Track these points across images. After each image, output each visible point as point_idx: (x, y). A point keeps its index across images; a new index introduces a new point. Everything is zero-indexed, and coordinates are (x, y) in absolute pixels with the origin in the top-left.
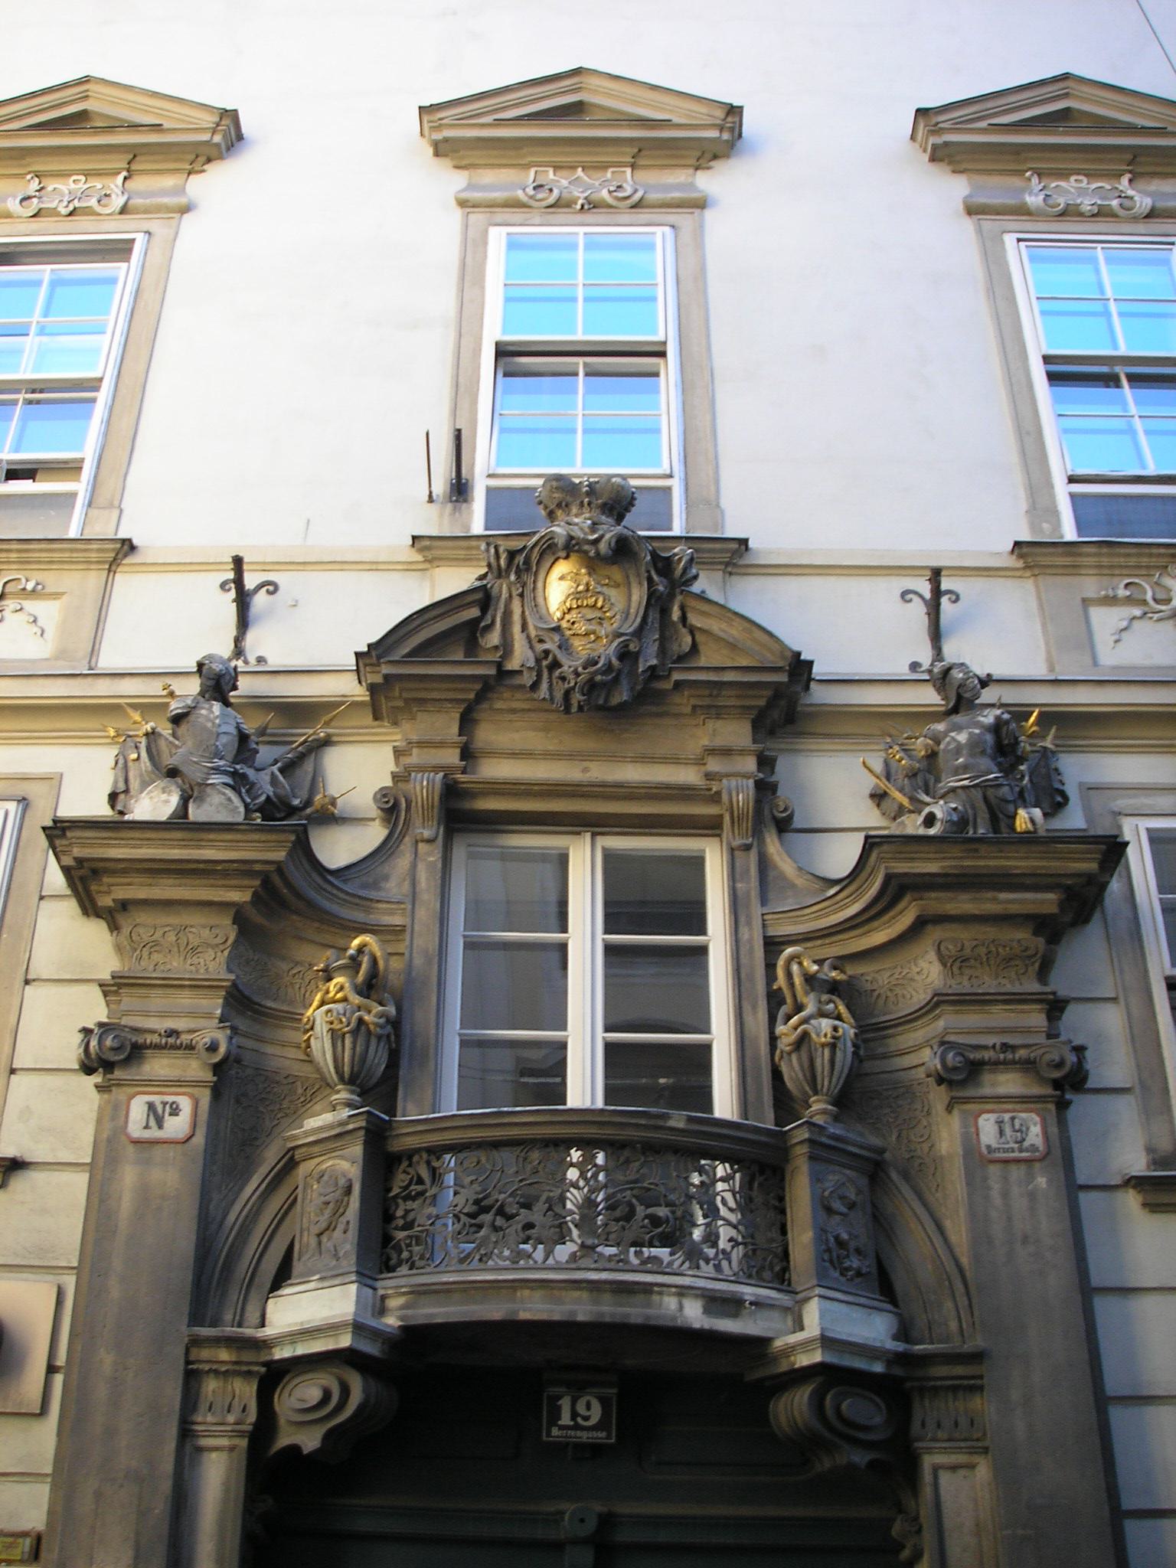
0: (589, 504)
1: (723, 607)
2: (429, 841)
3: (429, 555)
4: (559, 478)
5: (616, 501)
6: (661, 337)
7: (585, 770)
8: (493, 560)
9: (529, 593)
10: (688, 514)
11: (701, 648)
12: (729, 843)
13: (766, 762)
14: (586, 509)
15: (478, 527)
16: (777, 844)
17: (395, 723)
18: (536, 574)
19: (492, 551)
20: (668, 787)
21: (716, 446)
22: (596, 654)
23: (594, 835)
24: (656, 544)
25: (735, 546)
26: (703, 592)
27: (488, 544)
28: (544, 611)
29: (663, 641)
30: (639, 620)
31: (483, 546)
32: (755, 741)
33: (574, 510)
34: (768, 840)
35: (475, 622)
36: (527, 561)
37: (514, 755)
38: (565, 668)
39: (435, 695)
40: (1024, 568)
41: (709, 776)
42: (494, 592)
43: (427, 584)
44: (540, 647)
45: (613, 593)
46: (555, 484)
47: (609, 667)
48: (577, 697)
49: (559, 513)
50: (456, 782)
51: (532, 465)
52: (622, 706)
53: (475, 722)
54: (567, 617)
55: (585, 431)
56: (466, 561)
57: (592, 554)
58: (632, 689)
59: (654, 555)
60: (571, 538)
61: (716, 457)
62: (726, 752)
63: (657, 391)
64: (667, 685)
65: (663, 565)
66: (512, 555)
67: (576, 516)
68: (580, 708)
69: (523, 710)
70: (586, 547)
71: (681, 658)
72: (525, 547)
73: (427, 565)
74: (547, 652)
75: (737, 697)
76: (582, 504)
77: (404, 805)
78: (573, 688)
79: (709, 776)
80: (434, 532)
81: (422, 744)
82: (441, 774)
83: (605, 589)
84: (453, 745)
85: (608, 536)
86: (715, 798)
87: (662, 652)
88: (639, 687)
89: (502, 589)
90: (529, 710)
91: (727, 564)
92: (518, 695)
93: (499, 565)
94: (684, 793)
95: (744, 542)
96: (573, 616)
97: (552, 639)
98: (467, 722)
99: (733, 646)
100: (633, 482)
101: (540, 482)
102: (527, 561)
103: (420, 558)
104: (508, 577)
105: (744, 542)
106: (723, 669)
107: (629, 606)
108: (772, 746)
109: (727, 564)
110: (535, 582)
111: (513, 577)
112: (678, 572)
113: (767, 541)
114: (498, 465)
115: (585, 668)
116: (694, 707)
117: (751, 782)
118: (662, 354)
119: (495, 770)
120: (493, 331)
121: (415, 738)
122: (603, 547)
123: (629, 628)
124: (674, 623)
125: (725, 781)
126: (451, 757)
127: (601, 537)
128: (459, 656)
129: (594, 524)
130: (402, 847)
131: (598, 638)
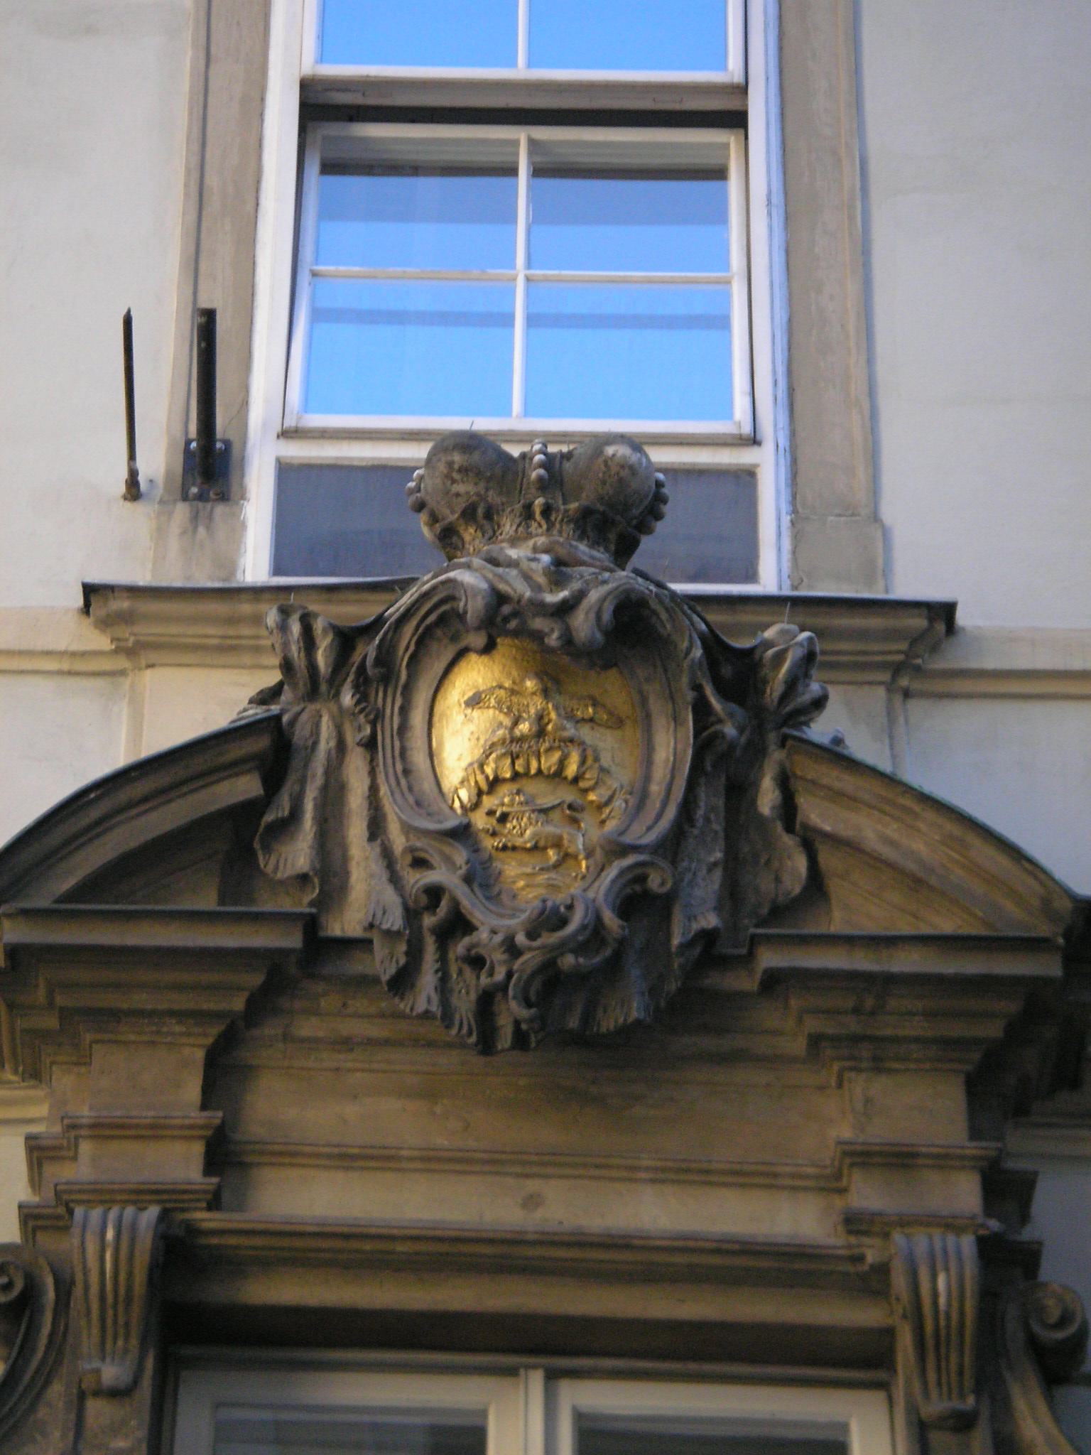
0: (547, 511)
1: (889, 780)
2: (116, 1394)
3: (128, 634)
4: (469, 442)
5: (613, 504)
6: (733, 72)
7: (532, 1202)
8: (295, 652)
9: (391, 737)
10: (797, 537)
11: (836, 887)
12: (912, 1409)
13: (1006, 1190)
14: (538, 526)
15: (255, 566)
16: (1042, 1408)
17: (35, 1074)
18: (408, 690)
19: (296, 628)
20: (748, 1248)
21: (870, 362)
22: (560, 898)
23: (552, 1376)
24: (714, 617)
25: (918, 622)
26: (838, 741)
27: (285, 612)
28: (428, 786)
29: (733, 867)
30: (671, 812)
31: (272, 617)
32: (975, 1133)
33: (508, 527)
34: (1020, 1404)
35: (248, 812)
36: (385, 659)
37: (348, 1159)
38: (483, 935)
39: (141, 1000)
40: (116, 651)
41: (854, 1223)
42: (300, 734)
43: (123, 711)
44: (417, 880)
45: (606, 742)
46: (457, 458)
47: (596, 929)
48: (511, 1011)
49: (469, 533)
50: (192, 1230)
51: (398, 413)
52: (628, 1032)
53: (247, 1072)
54: (488, 802)
55: (532, 321)
56: (224, 651)
57: (553, 640)
58: (653, 991)
59: (714, 645)
60: (500, 598)
61: (872, 392)
62: (899, 1160)
63: (721, 217)
64: (744, 982)
65: (735, 671)
66: (347, 638)
67: (514, 542)
68: (521, 1040)
69: (371, 1042)
70: (538, 623)
71: (781, 911)
72: (379, 621)
73: (122, 662)
74: (434, 893)
75: (930, 1015)
76: (528, 513)
77: (50, 1295)
78: (503, 987)
79: (854, 1223)
80: (143, 577)
81: (104, 1130)
82: (153, 1212)
83: (586, 733)
84: (185, 1133)
85: (594, 595)
86: (873, 1282)
87: (732, 894)
88: (673, 986)
89: (322, 727)
90: (387, 1043)
91: (897, 669)
92: (360, 1004)
93: (312, 667)
94: (787, 1266)
95: (944, 613)
96: (503, 799)
97: (448, 860)
98: (223, 1073)
99: (916, 883)
100: (659, 456)
101: (418, 452)
102: (385, 659)
103: (102, 642)
104: (337, 695)
105: (944, 613)
106: (891, 941)
107: (647, 779)
108: (1023, 1147)
109: (897, 669)
110: (405, 711)
111: (347, 699)
112: (776, 687)
113: (992, 613)
114: (306, 407)
115: (532, 935)
116: (815, 1041)
117: (968, 1243)
118: (736, 120)
119: (298, 1198)
120: (295, 50)
121: (85, 1113)
122: (583, 624)
123: (647, 832)
124: (761, 822)
125: (898, 1237)
126: (182, 1164)
127: (580, 596)
128: (207, 901)
129: (559, 563)
130: (42, 1412)
131: (567, 856)
